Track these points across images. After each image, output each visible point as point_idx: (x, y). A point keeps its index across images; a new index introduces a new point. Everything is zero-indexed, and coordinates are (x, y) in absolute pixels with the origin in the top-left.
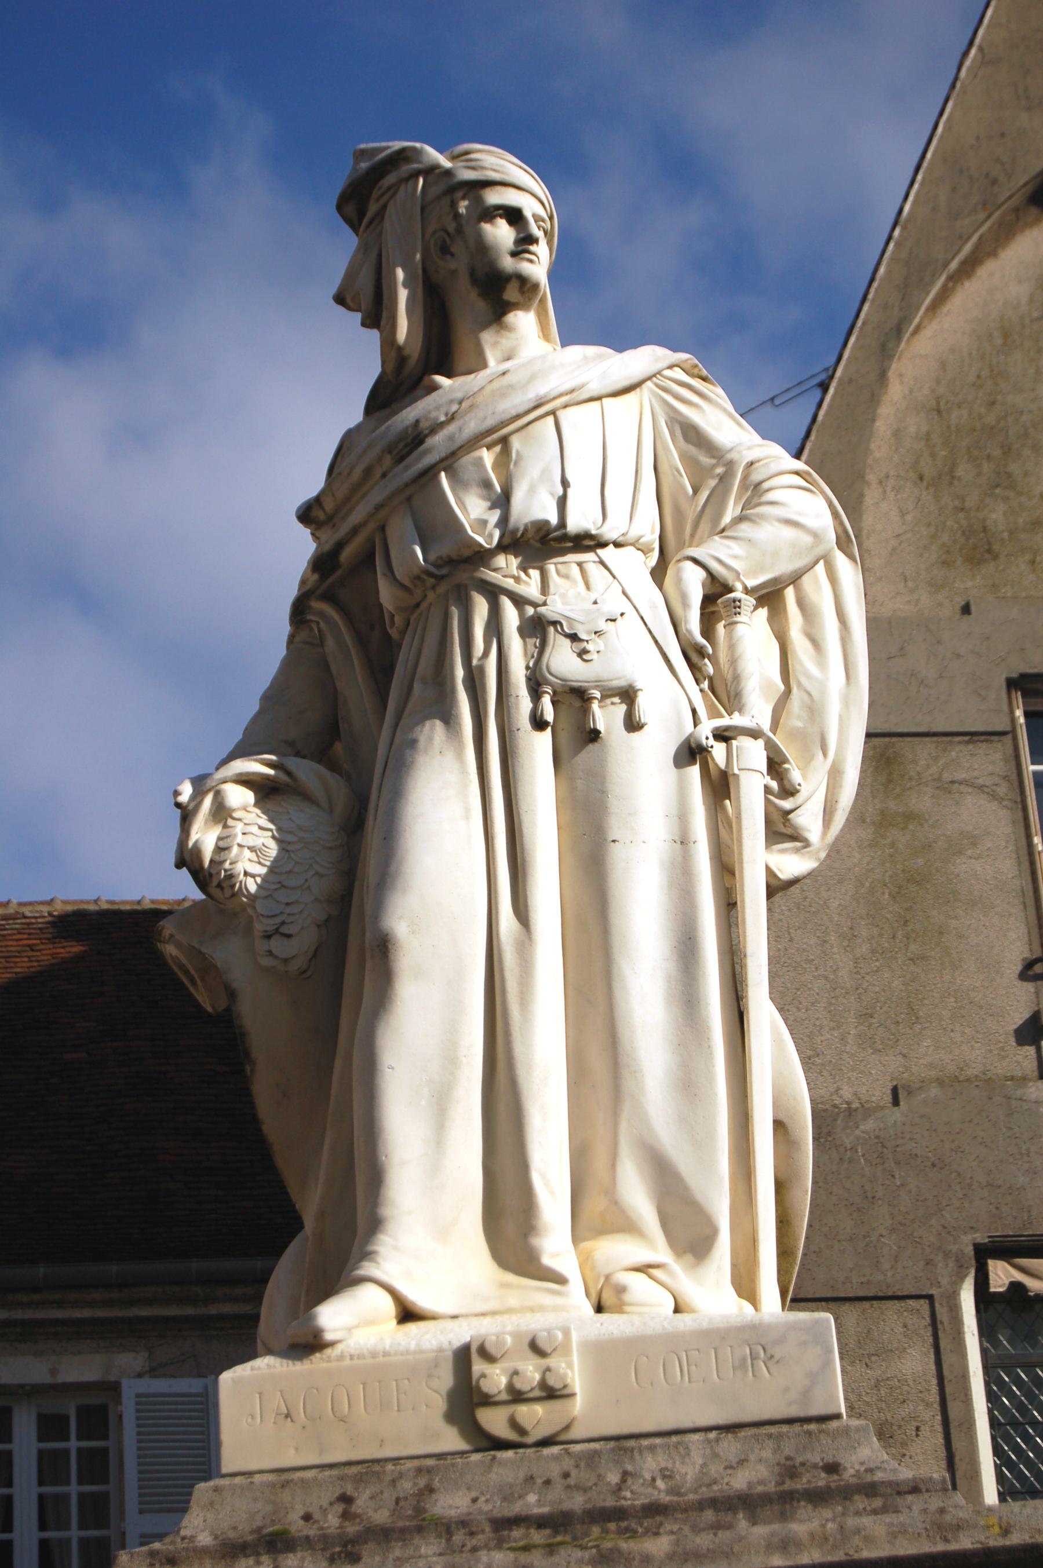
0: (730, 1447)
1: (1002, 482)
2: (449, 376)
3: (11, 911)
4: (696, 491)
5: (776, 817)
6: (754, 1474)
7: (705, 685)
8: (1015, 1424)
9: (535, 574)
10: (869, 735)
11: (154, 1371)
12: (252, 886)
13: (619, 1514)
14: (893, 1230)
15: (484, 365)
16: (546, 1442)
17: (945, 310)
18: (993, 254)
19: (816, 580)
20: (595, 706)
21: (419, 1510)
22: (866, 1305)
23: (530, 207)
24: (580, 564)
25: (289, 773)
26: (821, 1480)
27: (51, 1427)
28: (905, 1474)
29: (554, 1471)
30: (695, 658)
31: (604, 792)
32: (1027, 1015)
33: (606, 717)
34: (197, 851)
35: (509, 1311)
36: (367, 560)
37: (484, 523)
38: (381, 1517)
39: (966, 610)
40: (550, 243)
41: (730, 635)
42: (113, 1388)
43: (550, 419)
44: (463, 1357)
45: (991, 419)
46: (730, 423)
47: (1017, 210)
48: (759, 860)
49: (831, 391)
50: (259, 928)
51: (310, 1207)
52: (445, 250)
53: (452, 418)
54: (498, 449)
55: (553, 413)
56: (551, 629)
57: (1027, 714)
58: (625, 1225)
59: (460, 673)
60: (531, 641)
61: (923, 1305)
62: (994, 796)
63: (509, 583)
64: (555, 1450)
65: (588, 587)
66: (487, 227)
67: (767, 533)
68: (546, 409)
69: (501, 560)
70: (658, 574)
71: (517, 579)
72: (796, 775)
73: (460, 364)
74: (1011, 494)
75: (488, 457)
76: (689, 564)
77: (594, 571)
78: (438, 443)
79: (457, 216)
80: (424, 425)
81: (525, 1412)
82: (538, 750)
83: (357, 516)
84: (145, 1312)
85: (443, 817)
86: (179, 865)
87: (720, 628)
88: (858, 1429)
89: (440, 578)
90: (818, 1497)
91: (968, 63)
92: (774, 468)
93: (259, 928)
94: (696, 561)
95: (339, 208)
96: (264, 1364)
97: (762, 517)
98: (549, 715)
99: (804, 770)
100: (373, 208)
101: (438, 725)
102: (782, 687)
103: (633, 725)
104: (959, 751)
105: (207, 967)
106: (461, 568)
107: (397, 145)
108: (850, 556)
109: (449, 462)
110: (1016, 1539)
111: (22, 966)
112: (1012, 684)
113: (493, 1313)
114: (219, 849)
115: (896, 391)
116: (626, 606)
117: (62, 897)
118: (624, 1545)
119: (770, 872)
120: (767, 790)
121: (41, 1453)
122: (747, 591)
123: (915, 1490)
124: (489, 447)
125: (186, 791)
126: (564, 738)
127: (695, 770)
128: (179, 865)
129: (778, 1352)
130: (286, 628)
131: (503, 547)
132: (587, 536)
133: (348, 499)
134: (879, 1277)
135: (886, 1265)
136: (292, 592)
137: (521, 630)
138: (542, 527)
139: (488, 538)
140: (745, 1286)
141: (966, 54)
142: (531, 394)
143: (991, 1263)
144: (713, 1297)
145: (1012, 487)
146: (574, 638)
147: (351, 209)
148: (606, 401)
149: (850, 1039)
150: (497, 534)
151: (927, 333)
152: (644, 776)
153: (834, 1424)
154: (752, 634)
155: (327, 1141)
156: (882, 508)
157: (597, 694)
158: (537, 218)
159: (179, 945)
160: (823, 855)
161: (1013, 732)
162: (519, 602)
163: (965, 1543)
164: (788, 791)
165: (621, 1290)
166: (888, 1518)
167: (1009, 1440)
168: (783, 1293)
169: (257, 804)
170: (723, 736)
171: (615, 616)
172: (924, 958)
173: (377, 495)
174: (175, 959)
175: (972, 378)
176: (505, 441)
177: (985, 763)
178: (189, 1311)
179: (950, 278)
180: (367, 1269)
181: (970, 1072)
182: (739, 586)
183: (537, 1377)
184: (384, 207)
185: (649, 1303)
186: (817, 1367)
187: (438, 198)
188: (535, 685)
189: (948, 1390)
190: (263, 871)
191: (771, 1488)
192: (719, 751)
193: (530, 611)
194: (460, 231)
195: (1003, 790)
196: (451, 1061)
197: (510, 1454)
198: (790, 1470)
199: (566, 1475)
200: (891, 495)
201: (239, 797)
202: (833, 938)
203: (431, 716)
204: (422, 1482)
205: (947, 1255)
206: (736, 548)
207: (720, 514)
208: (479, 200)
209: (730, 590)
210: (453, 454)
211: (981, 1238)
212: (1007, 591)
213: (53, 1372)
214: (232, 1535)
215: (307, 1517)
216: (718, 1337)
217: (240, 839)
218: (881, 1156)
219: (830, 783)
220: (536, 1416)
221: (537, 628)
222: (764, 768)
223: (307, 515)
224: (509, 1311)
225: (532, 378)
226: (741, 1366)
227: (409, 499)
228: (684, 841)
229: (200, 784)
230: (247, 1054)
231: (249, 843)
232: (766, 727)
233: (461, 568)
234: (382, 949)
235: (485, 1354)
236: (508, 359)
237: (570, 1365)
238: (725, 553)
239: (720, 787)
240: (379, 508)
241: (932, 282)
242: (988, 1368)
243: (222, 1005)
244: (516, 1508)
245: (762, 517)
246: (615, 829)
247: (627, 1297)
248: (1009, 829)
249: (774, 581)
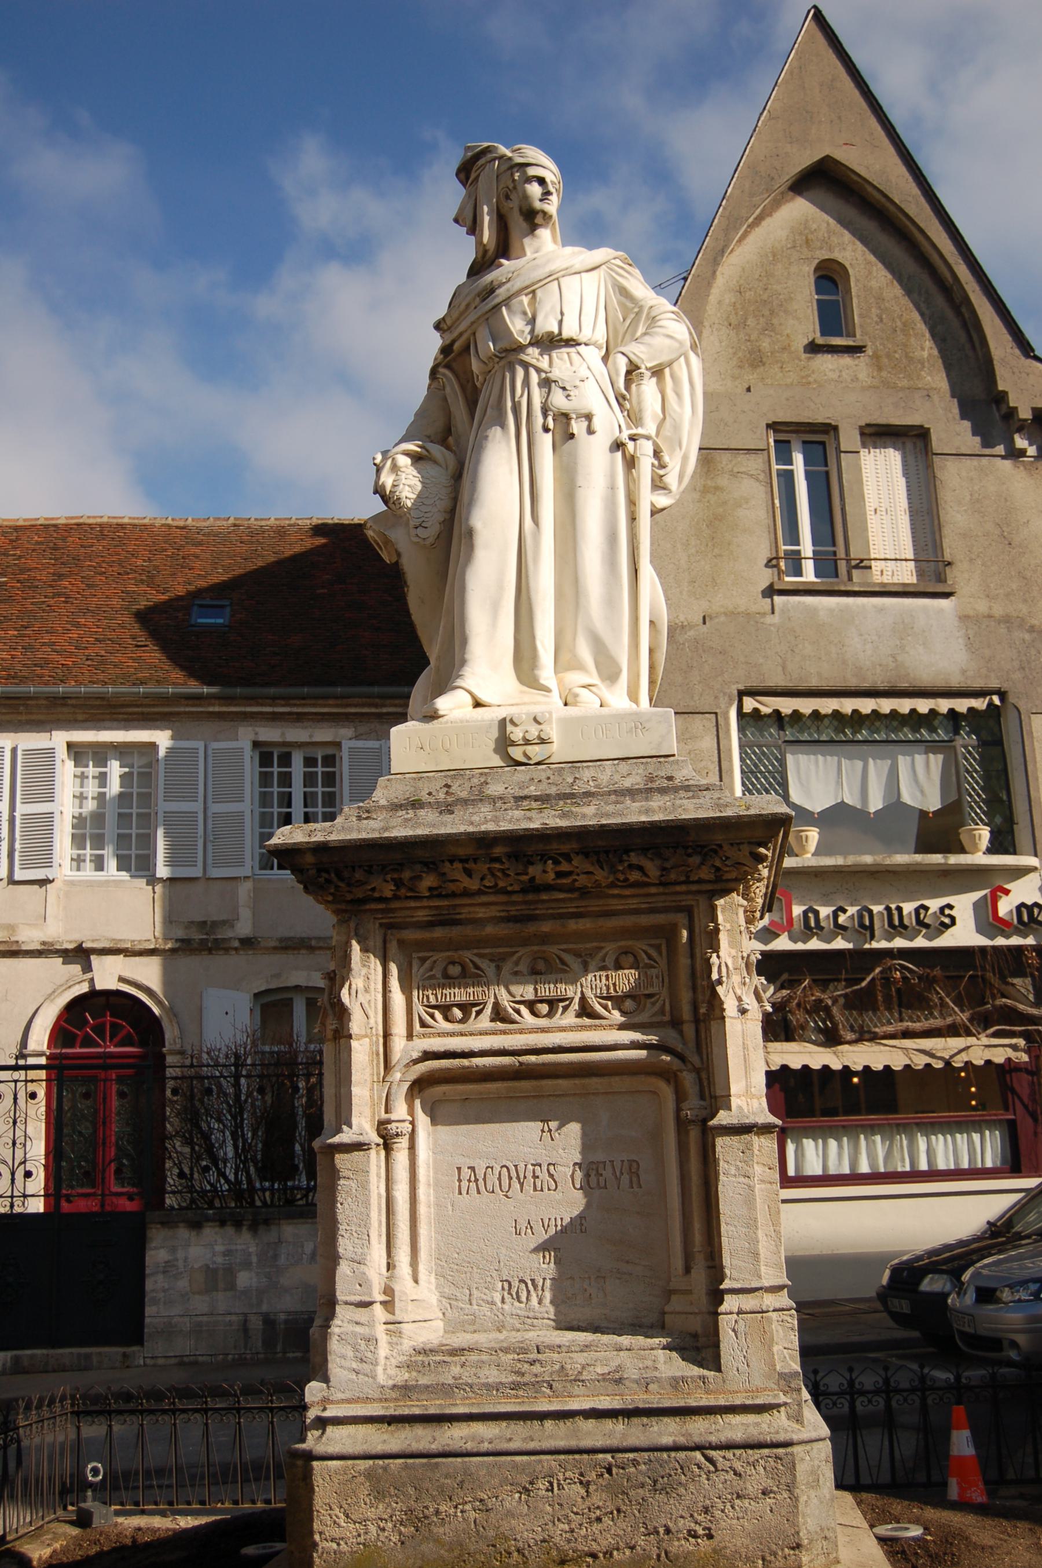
0: (624, 767)
1: (769, 328)
2: (508, 259)
3: (292, 522)
4: (624, 320)
5: (657, 479)
6: (635, 779)
7: (626, 413)
8: (752, 772)
9: (546, 357)
10: (700, 449)
11: (357, 737)
12: (409, 504)
13: (572, 796)
14: (700, 682)
15: (525, 255)
16: (538, 763)
17: (745, 242)
18: (770, 215)
19: (680, 365)
20: (573, 422)
21: (481, 792)
22: (686, 716)
23: (549, 177)
24: (568, 353)
25: (427, 451)
26: (665, 783)
27: (310, 762)
28: (704, 782)
29: (543, 777)
30: (621, 400)
31: (575, 463)
32: (768, 584)
33: (578, 427)
34: (383, 486)
35: (524, 704)
36: (466, 349)
37: (523, 332)
38: (464, 795)
39: (749, 390)
40: (558, 195)
41: (638, 390)
42: (338, 745)
43: (556, 282)
44: (503, 723)
45: (765, 297)
46: (640, 286)
47: (782, 193)
48: (647, 498)
49: (689, 280)
50: (412, 523)
51: (433, 653)
52: (507, 197)
53: (509, 280)
54: (530, 296)
55: (557, 279)
56: (553, 384)
57: (775, 441)
58: (578, 666)
59: (509, 404)
60: (544, 390)
61: (713, 716)
62: (757, 480)
63: (534, 362)
64: (544, 767)
65: (571, 364)
66: (527, 186)
67: (658, 341)
68: (554, 277)
69: (530, 350)
70: (605, 359)
71: (538, 360)
72: (666, 458)
73: (513, 253)
74: (772, 334)
75: (525, 300)
76: (620, 355)
77: (574, 356)
78: (502, 293)
79: (514, 180)
80: (495, 283)
81: (529, 749)
82: (545, 442)
83: (462, 327)
84: (353, 710)
85: (499, 471)
86: (376, 492)
87: (633, 387)
88: (683, 761)
89: (501, 358)
90: (663, 791)
91: (762, 118)
92: (662, 309)
93: (412, 523)
94: (623, 354)
95: (457, 175)
96: (411, 725)
97: (657, 334)
98: (551, 425)
99: (670, 456)
100: (473, 176)
101: (498, 428)
102: (661, 416)
103: (590, 431)
104: (742, 458)
105: (387, 541)
106: (510, 354)
107: (486, 144)
108: (697, 354)
109: (507, 301)
110: (752, 812)
111: (297, 549)
112: (768, 426)
113: (517, 704)
114: (394, 486)
115: (720, 281)
116: (588, 374)
117: (315, 516)
118: (573, 809)
119: (652, 504)
120: (653, 465)
121: (305, 773)
122: (647, 369)
123: (707, 789)
124: (526, 295)
125: (379, 458)
126: (557, 437)
127: (619, 454)
128: (376, 492)
129: (647, 726)
130: (428, 381)
131: (531, 344)
132: (572, 340)
133: (458, 319)
134: (692, 703)
135: (696, 698)
136: (431, 364)
137: (539, 384)
138: (550, 334)
139: (524, 339)
140: (633, 695)
141: (761, 114)
142: (547, 270)
143: (745, 698)
144: (618, 700)
145: (773, 330)
146: (564, 389)
147: (462, 176)
148: (584, 275)
149: (685, 593)
150: (529, 337)
151: (735, 253)
152: (595, 456)
153: (672, 759)
154: (648, 388)
155: (442, 624)
156: (712, 339)
157: (574, 416)
158: (553, 183)
159: (374, 531)
160: (677, 497)
161: (768, 450)
162: (538, 370)
163: (729, 813)
164: (663, 466)
165: (576, 696)
166: (694, 801)
167: (749, 779)
168: (651, 700)
169: (412, 465)
170: (633, 438)
171: (584, 379)
172: (720, 555)
173: (472, 317)
174: (373, 537)
175: (757, 277)
176: (534, 292)
177: (754, 464)
178: (373, 710)
179: (749, 226)
180: (459, 682)
181: (740, 610)
182: (643, 367)
183: (537, 734)
184: (478, 176)
185: (589, 701)
186: (664, 732)
187: (505, 171)
188: (545, 412)
189: (722, 756)
190: (414, 496)
191: (641, 786)
192: (630, 445)
193: (543, 375)
194: (515, 188)
195: (762, 477)
196: (501, 588)
197: (523, 768)
198: (651, 779)
199: (549, 778)
200: (716, 333)
201: (404, 461)
202: (679, 546)
203: (495, 425)
204: (482, 780)
205: (725, 694)
206: (642, 348)
207: (635, 331)
208: (525, 173)
209: (639, 368)
210: (509, 298)
211: (741, 687)
212: (769, 381)
213: (311, 736)
214: (396, 800)
215: (430, 794)
216: (621, 717)
217: (404, 481)
218: (696, 647)
219: (682, 464)
220: (536, 752)
221: (547, 383)
222: (651, 453)
223: (438, 326)
224: (524, 704)
225: (548, 261)
226: (631, 731)
227: (487, 319)
228: (612, 488)
229: (385, 454)
230: (405, 583)
231: (408, 483)
232: (653, 434)
233: (510, 354)
234: (470, 533)
235: (512, 721)
236: (537, 252)
237: (552, 729)
238: (638, 351)
239: (631, 462)
240: (473, 323)
241: (740, 229)
242: (741, 747)
243: (394, 561)
244: (526, 792)
245: (657, 334)
246: (580, 481)
247: (578, 699)
248: (763, 496)
249: (660, 365)
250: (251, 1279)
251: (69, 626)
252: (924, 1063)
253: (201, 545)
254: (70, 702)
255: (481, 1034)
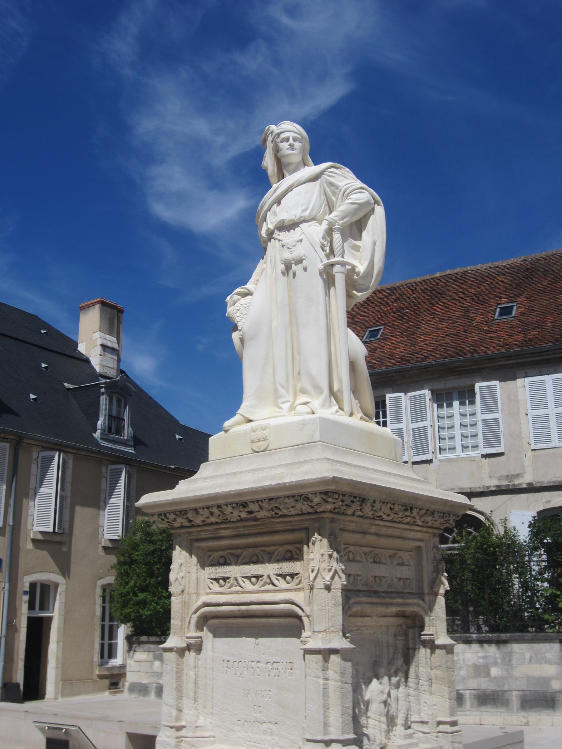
250: (498, 671)
251: (433, 330)
252: (18, 681)
253: (505, 274)
254: (429, 369)
255: (270, 590)
